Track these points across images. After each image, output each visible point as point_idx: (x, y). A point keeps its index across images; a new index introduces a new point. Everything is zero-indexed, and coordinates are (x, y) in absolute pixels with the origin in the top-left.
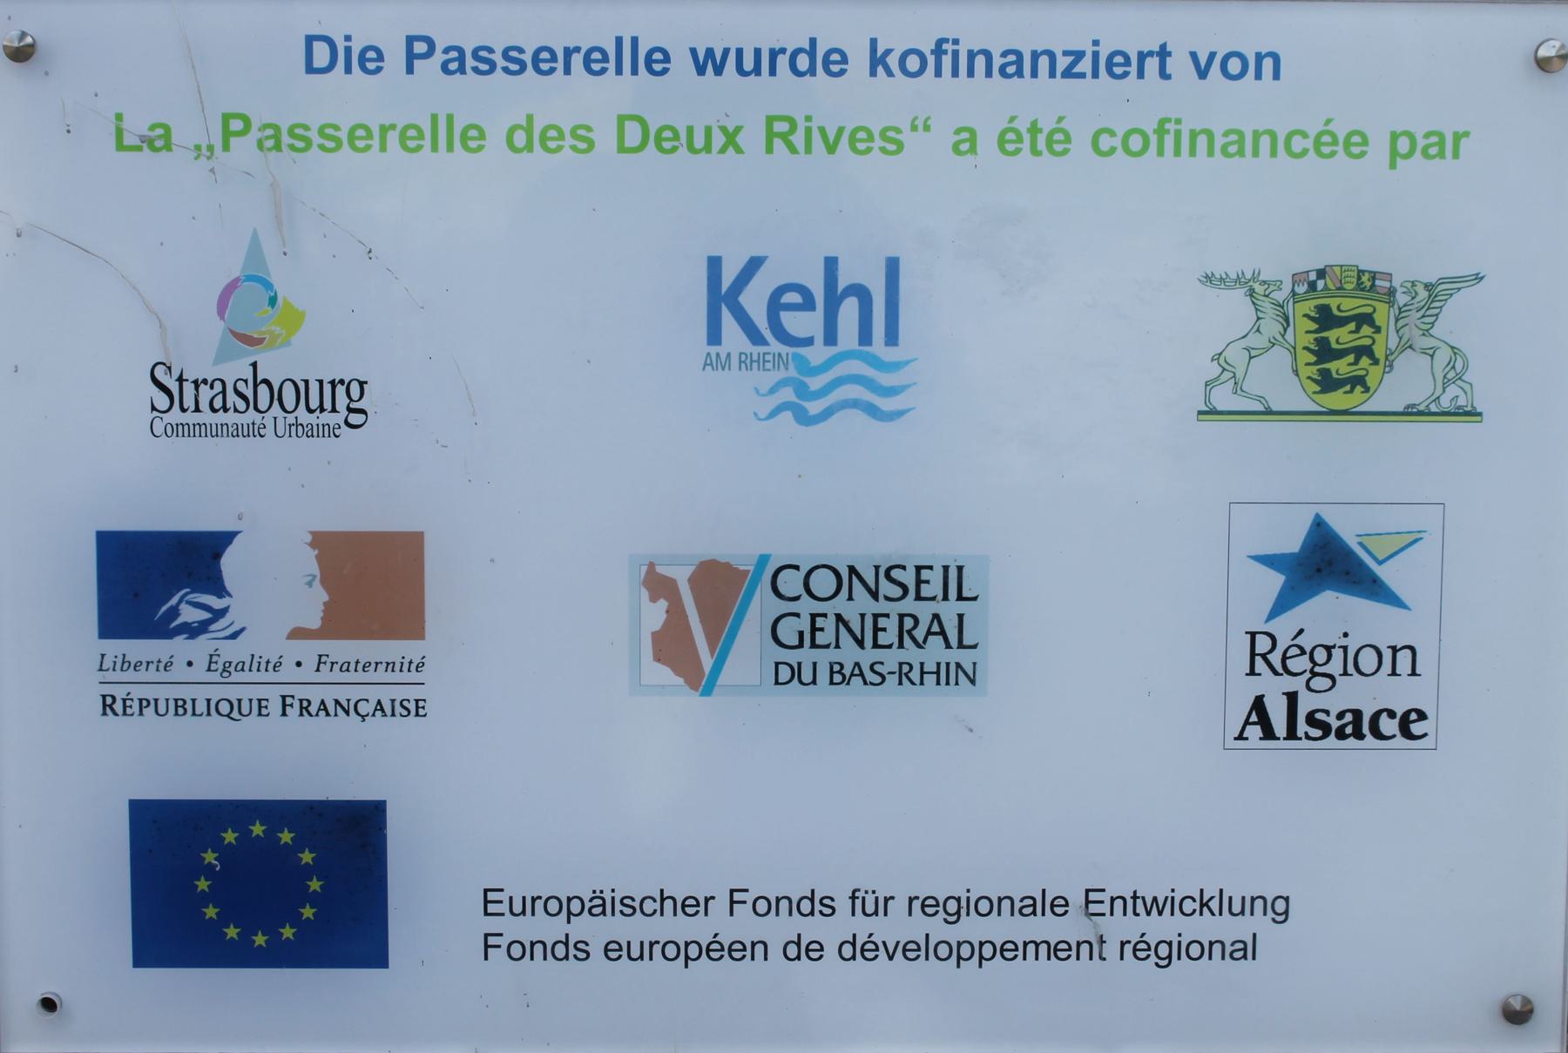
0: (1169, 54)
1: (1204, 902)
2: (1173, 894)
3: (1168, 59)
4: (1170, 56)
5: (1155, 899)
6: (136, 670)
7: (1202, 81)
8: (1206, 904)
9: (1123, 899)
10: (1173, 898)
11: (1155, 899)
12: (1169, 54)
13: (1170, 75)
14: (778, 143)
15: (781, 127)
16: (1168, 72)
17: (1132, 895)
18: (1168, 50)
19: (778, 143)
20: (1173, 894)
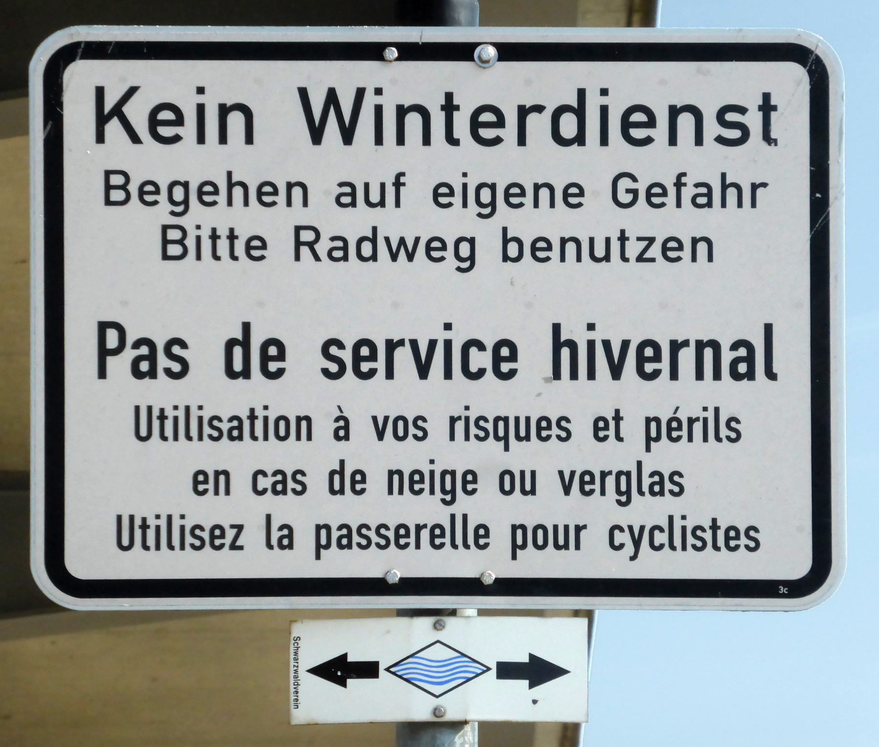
0: (622, 419)
1: (108, 107)
2: (448, 335)
3: (621, 421)
4: (257, 419)
5: (402, 241)
6: (273, 376)
7: (317, 147)
8: (118, 111)
9: (422, 110)
10: (448, 344)
11: (402, 241)
12: (622, 419)
13: (623, 438)
14: (305, 251)
15: (307, 236)
16: (456, 136)
17: (443, 102)
18: (626, 236)
19: (305, 251)
20: (448, 335)
